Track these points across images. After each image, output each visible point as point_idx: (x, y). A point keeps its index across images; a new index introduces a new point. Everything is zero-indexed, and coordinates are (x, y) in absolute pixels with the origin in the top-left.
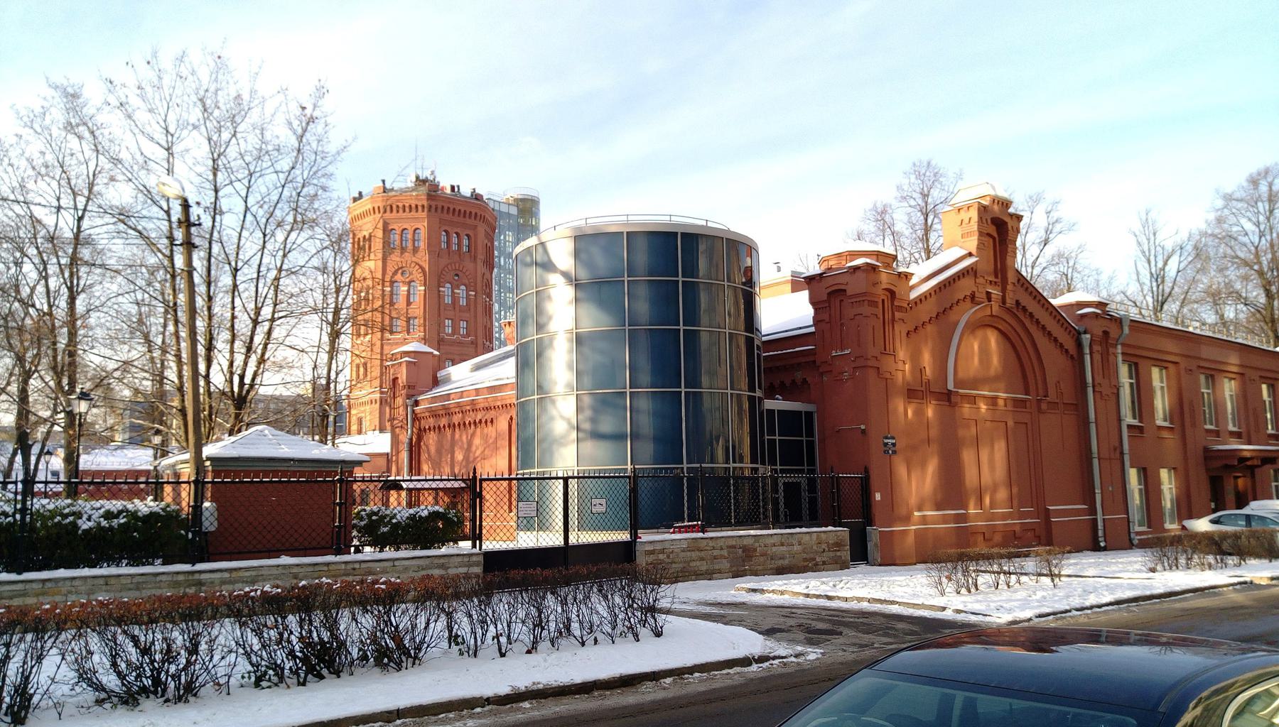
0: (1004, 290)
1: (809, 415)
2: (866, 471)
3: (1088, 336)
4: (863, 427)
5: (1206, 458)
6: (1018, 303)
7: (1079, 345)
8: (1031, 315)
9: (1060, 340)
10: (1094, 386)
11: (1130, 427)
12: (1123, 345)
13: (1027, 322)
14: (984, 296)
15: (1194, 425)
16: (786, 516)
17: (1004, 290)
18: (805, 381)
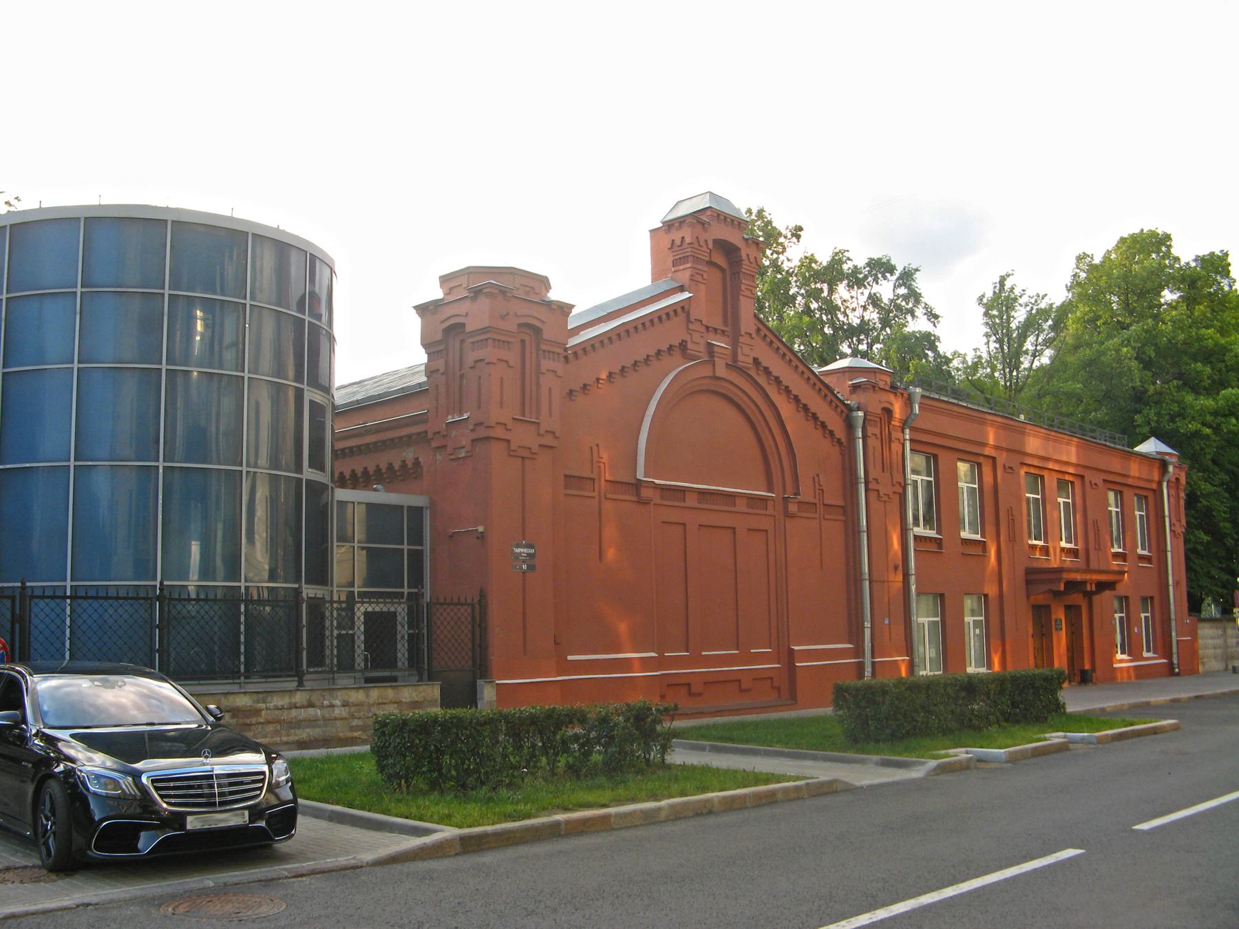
0: (735, 344)
1: (416, 512)
2: (483, 595)
3: (861, 414)
4: (481, 529)
5: (1028, 582)
6: (756, 361)
7: (850, 425)
8: (778, 381)
9: (822, 417)
10: (867, 483)
11: (918, 538)
12: (912, 429)
13: (762, 380)
14: (702, 348)
15: (1098, 549)
16: (366, 659)
17: (735, 344)
18: (417, 463)
